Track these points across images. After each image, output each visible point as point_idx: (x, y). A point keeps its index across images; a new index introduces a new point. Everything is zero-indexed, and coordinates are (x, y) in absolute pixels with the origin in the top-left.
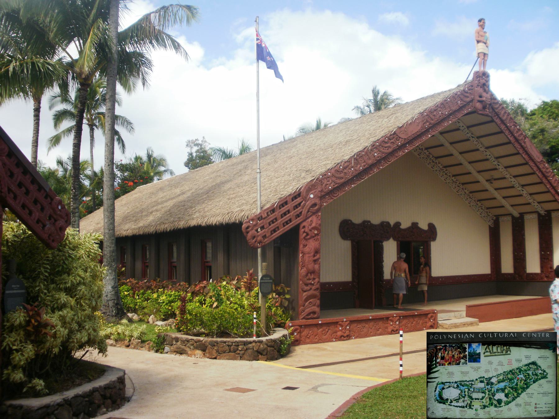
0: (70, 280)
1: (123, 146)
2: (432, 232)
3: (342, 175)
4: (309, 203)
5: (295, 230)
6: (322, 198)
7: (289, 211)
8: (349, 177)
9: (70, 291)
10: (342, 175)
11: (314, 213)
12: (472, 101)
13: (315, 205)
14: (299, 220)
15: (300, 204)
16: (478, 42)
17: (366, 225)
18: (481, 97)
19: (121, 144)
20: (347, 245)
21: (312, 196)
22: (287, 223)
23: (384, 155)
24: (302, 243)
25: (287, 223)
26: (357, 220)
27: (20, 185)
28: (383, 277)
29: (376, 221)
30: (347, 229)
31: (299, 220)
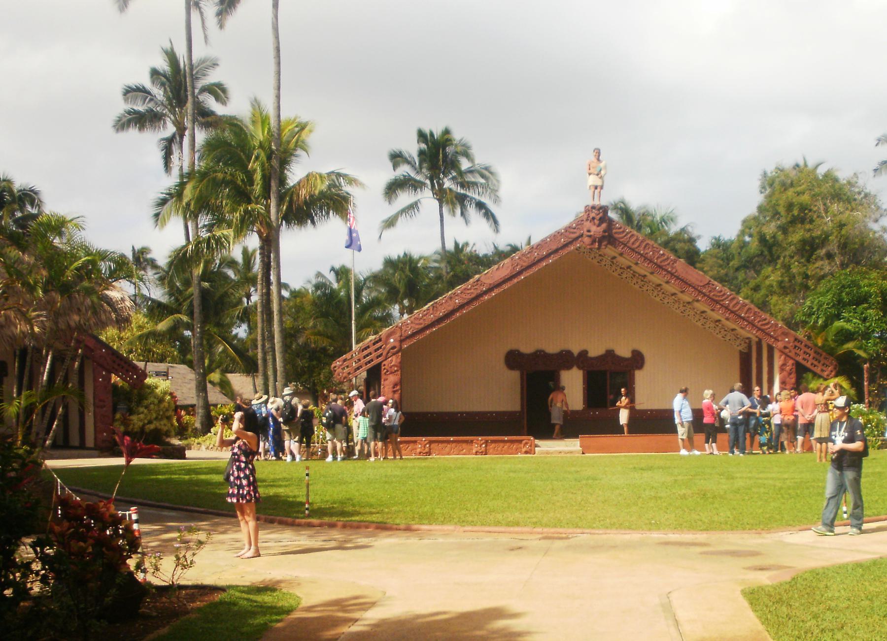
0: (146, 402)
1: (496, 222)
2: (637, 360)
3: (421, 321)
4: (389, 346)
5: (378, 366)
6: (401, 341)
7: (370, 354)
8: (427, 323)
9: (146, 407)
10: (421, 321)
11: (394, 354)
12: (582, 236)
13: (393, 348)
14: (380, 359)
15: (380, 347)
16: (590, 174)
17: (540, 355)
18: (589, 231)
19: (491, 220)
20: (515, 375)
21: (392, 340)
22: (369, 362)
23: (465, 301)
24: (383, 377)
25: (369, 362)
26: (527, 349)
27: (119, 365)
28: (515, 412)
29: (552, 348)
30: (513, 359)
31: (380, 359)
